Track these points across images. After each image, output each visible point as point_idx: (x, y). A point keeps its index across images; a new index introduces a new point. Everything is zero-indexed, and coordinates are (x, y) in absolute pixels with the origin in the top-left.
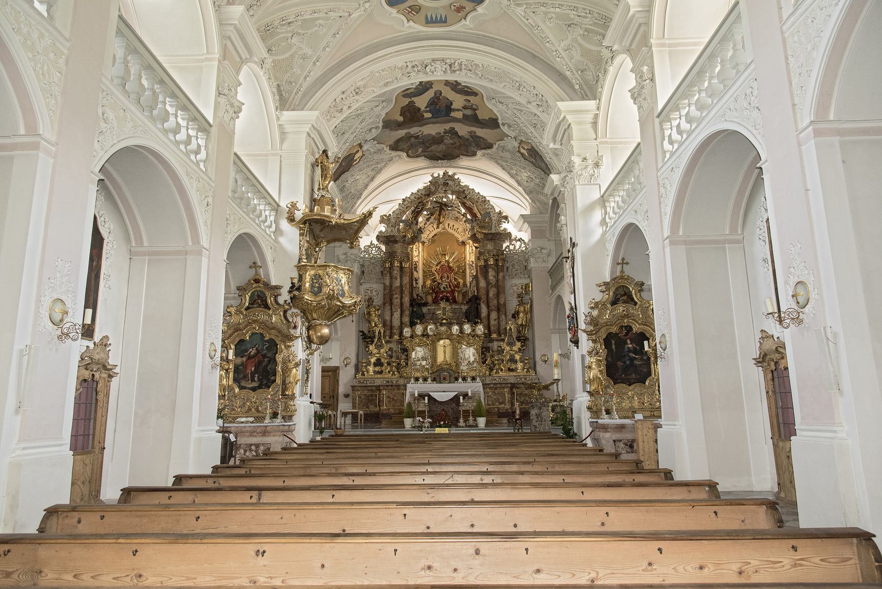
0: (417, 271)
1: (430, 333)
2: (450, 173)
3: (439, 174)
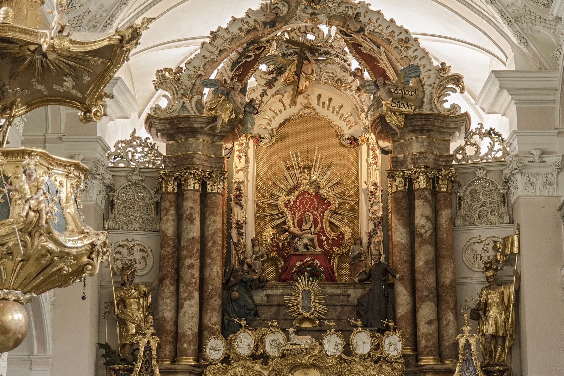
0: (241, 206)
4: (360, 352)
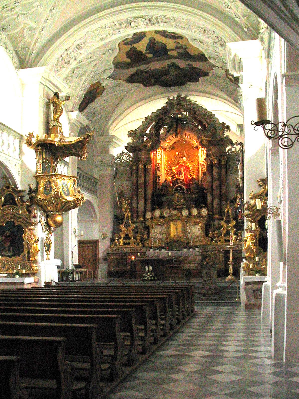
2: (183, 96)
3: (174, 97)
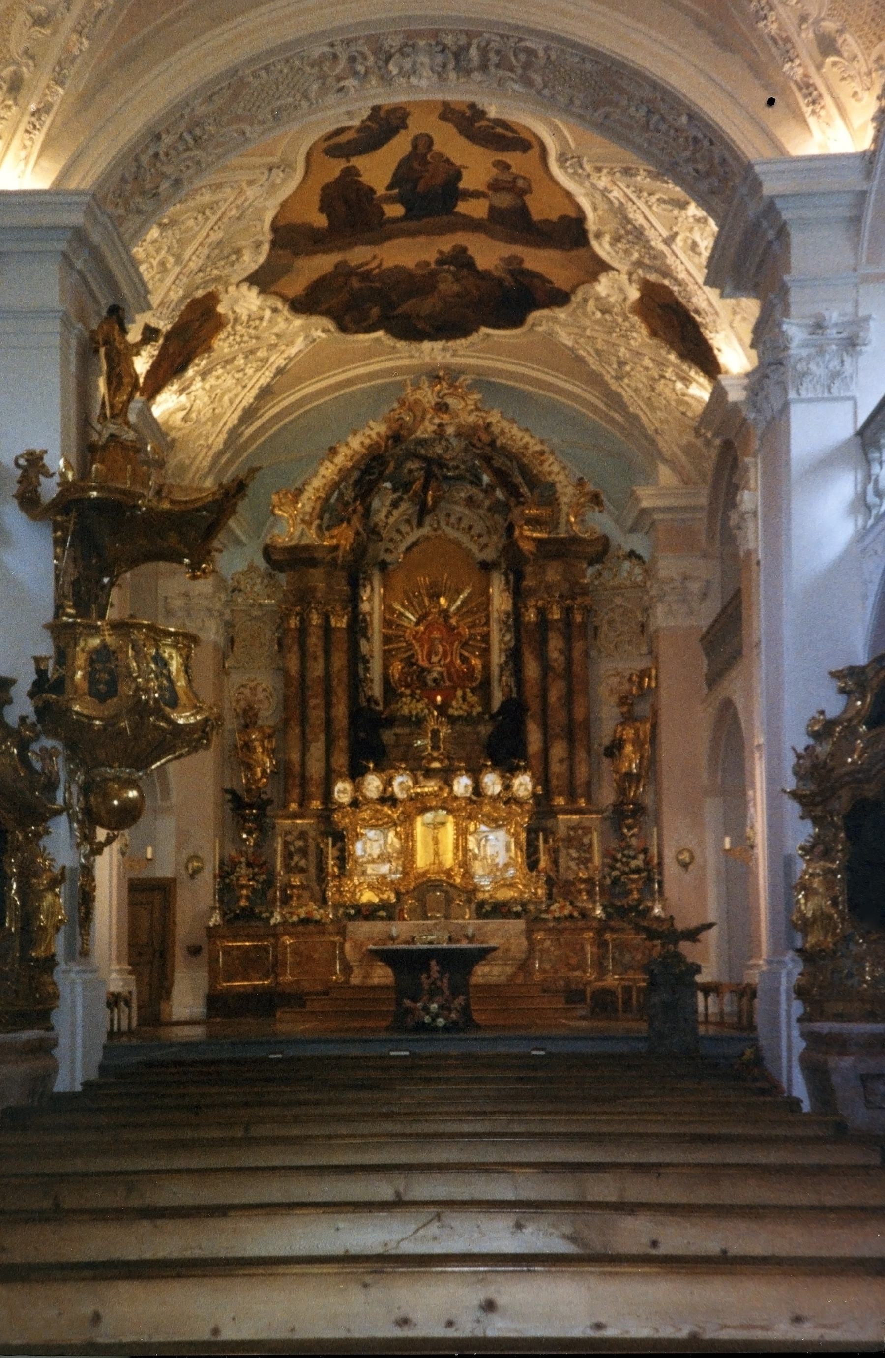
1: (400, 795)
4: (489, 793)
